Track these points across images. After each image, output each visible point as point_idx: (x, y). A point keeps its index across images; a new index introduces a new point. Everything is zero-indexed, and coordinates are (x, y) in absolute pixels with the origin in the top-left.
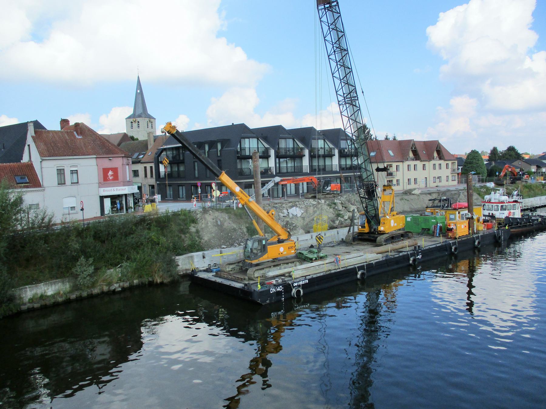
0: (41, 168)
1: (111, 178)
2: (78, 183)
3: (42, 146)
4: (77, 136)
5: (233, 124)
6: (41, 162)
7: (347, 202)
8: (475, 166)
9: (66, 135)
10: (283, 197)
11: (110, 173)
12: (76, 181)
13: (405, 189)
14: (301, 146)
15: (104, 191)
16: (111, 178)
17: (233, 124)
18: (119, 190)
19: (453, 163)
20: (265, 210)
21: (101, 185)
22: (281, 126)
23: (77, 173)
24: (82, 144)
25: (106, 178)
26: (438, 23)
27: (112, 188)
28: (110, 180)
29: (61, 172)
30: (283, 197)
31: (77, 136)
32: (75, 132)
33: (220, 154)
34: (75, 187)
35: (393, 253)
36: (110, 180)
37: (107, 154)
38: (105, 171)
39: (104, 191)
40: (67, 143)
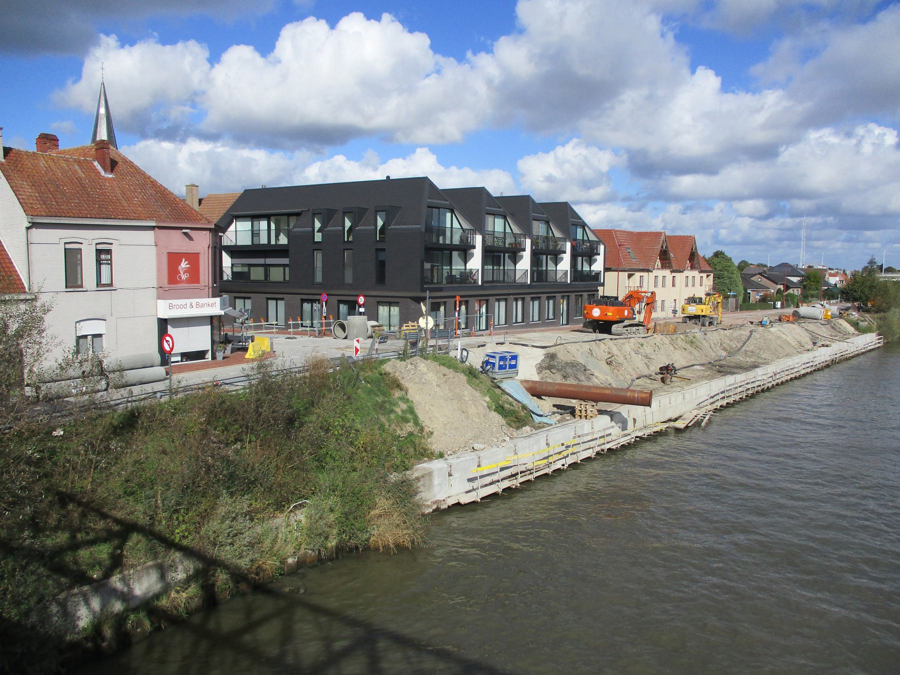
0: (28, 244)
1: (184, 277)
2: (111, 285)
3: (28, 190)
4: (103, 173)
5: (388, 177)
6: (28, 228)
7: (633, 354)
8: (727, 281)
9: (77, 167)
10: (487, 329)
11: (184, 265)
14: (558, 234)
15: (171, 307)
16: (184, 277)
17: (388, 177)
18: (203, 306)
19: (708, 276)
20: (398, 339)
21: (163, 293)
22: (426, 178)
23: (111, 264)
25: (173, 276)
26: (168, 47)
27: (188, 301)
28: (181, 282)
29: (72, 257)
30: (487, 329)
31: (103, 173)
32: (96, 163)
34: (104, 295)
36: (181, 282)
37: (177, 219)
38: (174, 259)
40: (84, 187)
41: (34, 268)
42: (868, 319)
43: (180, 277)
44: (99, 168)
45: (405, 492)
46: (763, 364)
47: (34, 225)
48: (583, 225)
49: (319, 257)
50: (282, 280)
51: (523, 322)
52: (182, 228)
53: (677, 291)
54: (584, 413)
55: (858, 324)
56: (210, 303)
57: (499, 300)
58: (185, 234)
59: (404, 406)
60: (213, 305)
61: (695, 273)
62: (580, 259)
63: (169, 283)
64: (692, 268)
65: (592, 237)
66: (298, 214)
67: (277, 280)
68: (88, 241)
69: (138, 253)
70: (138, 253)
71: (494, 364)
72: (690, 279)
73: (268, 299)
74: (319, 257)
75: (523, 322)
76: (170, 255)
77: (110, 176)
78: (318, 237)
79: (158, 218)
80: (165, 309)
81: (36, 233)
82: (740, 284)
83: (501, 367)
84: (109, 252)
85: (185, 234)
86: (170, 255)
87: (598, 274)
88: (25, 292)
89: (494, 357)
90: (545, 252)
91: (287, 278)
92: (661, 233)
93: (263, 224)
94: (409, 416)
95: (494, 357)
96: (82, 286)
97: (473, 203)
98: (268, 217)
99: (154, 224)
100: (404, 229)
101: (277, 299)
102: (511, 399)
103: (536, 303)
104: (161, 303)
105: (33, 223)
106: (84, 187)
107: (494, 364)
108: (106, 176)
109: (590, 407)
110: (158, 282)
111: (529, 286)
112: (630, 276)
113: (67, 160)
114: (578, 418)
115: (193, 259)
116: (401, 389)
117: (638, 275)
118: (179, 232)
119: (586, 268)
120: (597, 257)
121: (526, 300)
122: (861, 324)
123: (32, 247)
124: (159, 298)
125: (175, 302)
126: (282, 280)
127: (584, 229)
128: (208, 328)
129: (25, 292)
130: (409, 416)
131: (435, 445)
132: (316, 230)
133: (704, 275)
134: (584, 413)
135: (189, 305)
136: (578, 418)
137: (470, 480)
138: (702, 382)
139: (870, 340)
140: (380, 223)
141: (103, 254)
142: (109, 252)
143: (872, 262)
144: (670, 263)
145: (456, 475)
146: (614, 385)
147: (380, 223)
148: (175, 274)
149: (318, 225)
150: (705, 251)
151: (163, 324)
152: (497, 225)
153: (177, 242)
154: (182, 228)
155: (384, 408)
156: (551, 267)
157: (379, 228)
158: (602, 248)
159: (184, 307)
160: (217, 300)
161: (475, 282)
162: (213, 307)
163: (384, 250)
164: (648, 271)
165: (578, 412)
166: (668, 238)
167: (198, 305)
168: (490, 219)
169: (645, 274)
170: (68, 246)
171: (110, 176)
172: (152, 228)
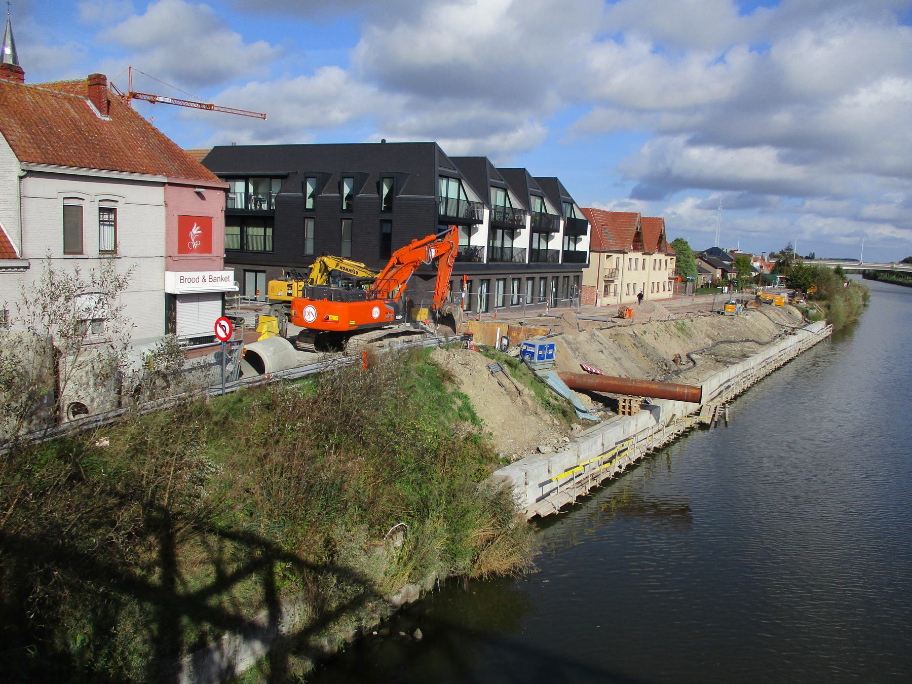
1: (195, 245)
2: (114, 252)
4: (98, 115)
5: (383, 141)
6: (21, 178)
8: (683, 265)
9: (68, 105)
11: (195, 231)
12: (109, 246)
13: (623, 302)
15: (182, 280)
16: (195, 245)
17: (383, 141)
18: (216, 280)
21: (171, 263)
22: (216, 147)
24: (119, 140)
25: (184, 245)
27: (201, 274)
29: (72, 216)
31: (98, 115)
32: (89, 102)
33: (348, 205)
35: (315, 366)
36: (192, 250)
38: (185, 222)
39: (182, 280)
41: (30, 227)
42: (817, 308)
43: (191, 245)
44: (93, 108)
45: (501, 505)
46: (752, 352)
47: (31, 173)
48: (572, 203)
49: (310, 225)
50: (262, 249)
51: (503, 306)
52: (195, 186)
53: (645, 276)
54: (627, 410)
55: (807, 311)
56: (224, 276)
57: (498, 280)
58: (199, 194)
59: (459, 403)
60: (226, 279)
61: (662, 257)
62: (499, 232)
63: (180, 252)
64: (660, 251)
65: (579, 216)
66: (283, 177)
67: (257, 249)
68: (91, 195)
69: (145, 213)
70: (145, 213)
71: (533, 354)
72: (633, 261)
73: (245, 271)
74: (310, 225)
75: (503, 306)
76: (181, 217)
77: (107, 119)
78: (309, 204)
79: (169, 174)
80: (174, 283)
81: (32, 183)
82: (713, 271)
83: (540, 358)
84: (112, 211)
85: (199, 194)
86: (181, 217)
87: (584, 254)
88: (16, 258)
89: (533, 346)
90: (543, 227)
91: (269, 248)
92: (636, 214)
93: (240, 186)
94: (466, 414)
95: (533, 346)
96: (82, 253)
97: (475, 170)
98: (246, 178)
99: (165, 181)
100: (416, 199)
101: (256, 272)
102: (554, 393)
103: (530, 283)
104: (170, 275)
105: (29, 172)
106: (80, 131)
107: (533, 354)
108: (103, 118)
109: (636, 402)
110: (167, 251)
111: (528, 266)
112: (608, 256)
113: (55, 96)
114: (621, 414)
115: (205, 223)
116: (452, 382)
117: (615, 256)
118: (192, 190)
119: (543, 246)
120: (583, 237)
121: (492, 282)
122: (811, 311)
123: (26, 201)
124: (167, 269)
125: (187, 275)
126: (262, 249)
127: (572, 208)
128: (219, 303)
129: (16, 258)
130: (466, 414)
131: (502, 448)
132: (308, 195)
133: (669, 258)
134: (627, 410)
135: (201, 278)
136: (621, 414)
137: (541, 485)
138: (707, 376)
139: (819, 330)
140: (347, 190)
141: (108, 213)
142: (112, 211)
143: (789, 249)
144: (642, 245)
145: (531, 483)
146: (623, 376)
147: (347, 190)
148: (186, 241)
149: (310, 189)
150: (670, 239)
151: (171, 300)
152: (498, 197)
153: (188, 202)
154: (195, 186)
155: (442, 404)
156: (507, 244)
157: (384, 196)
158: (589, 227)
159: (196, 280)
160: (230, 273)
161: (480, 260)
162: (225, 280)
163: (390, 221)
164: (624, 252)
165: (621, 409)
166: (643, 219)
167: (210, 278)
168: (493, 191)
169: (620, 256)
170: (68, 202)
171: (107, 119)
172: (163, 184)
